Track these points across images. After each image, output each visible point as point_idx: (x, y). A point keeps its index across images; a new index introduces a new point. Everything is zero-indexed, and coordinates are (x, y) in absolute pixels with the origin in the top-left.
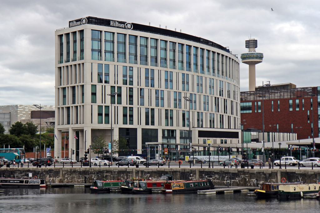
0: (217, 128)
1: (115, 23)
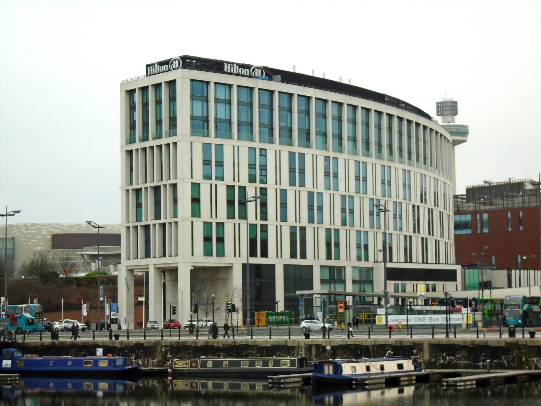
0: (417, 265)
1: (232, 67)
